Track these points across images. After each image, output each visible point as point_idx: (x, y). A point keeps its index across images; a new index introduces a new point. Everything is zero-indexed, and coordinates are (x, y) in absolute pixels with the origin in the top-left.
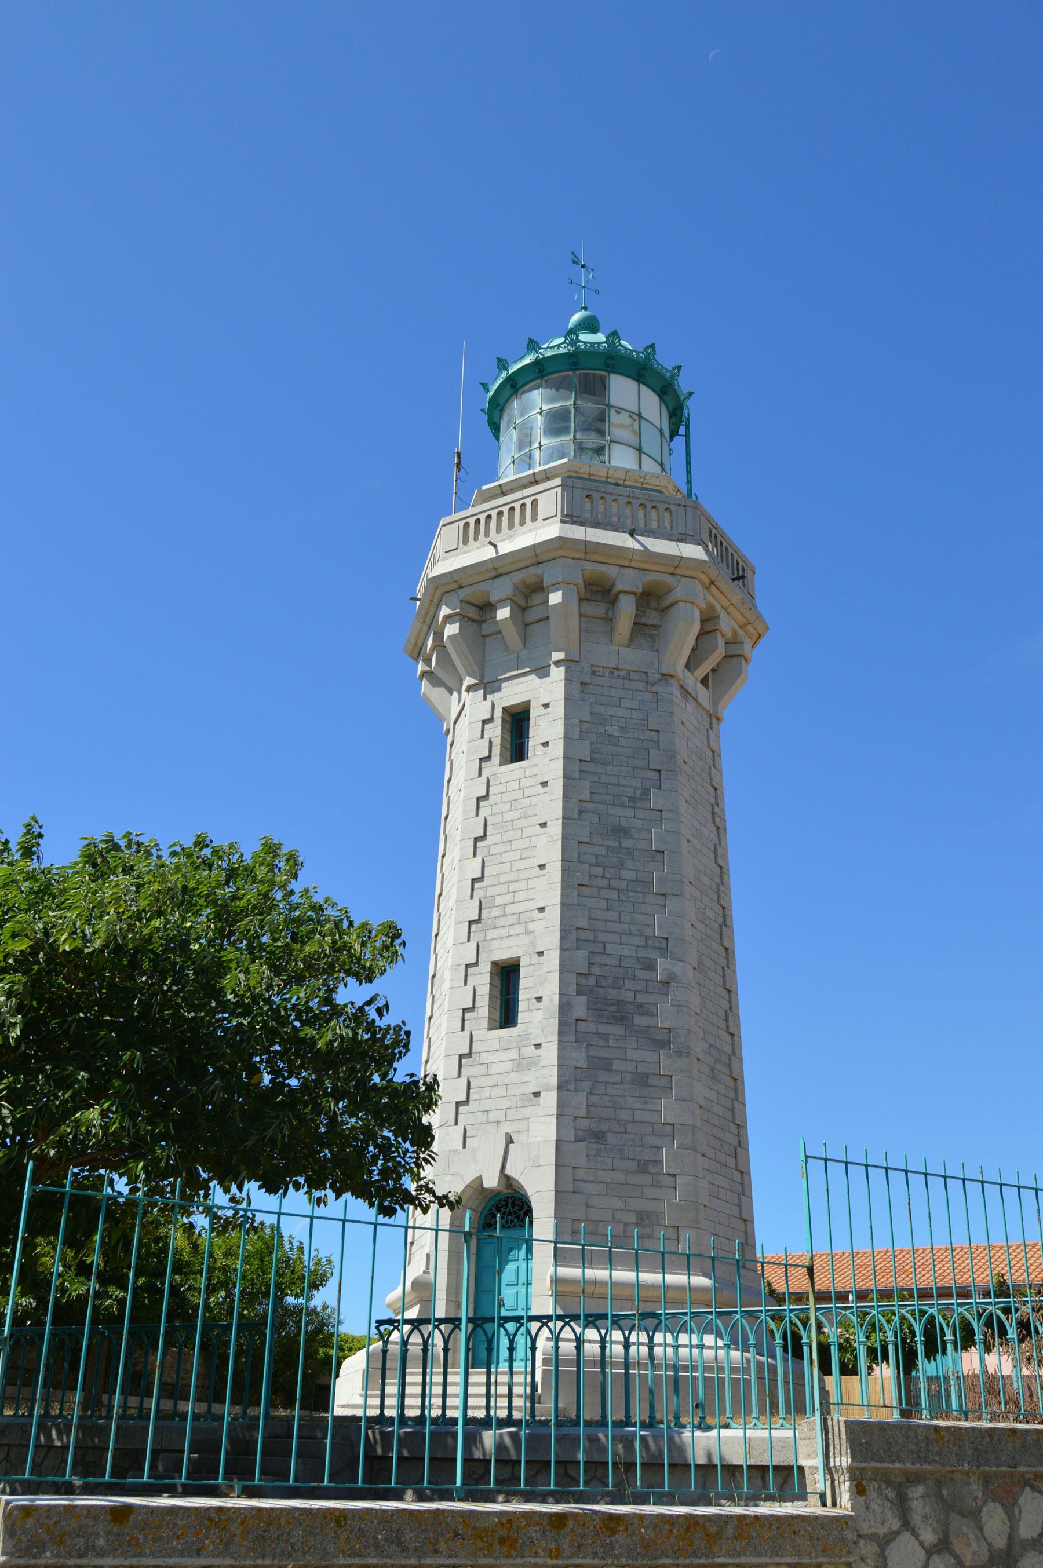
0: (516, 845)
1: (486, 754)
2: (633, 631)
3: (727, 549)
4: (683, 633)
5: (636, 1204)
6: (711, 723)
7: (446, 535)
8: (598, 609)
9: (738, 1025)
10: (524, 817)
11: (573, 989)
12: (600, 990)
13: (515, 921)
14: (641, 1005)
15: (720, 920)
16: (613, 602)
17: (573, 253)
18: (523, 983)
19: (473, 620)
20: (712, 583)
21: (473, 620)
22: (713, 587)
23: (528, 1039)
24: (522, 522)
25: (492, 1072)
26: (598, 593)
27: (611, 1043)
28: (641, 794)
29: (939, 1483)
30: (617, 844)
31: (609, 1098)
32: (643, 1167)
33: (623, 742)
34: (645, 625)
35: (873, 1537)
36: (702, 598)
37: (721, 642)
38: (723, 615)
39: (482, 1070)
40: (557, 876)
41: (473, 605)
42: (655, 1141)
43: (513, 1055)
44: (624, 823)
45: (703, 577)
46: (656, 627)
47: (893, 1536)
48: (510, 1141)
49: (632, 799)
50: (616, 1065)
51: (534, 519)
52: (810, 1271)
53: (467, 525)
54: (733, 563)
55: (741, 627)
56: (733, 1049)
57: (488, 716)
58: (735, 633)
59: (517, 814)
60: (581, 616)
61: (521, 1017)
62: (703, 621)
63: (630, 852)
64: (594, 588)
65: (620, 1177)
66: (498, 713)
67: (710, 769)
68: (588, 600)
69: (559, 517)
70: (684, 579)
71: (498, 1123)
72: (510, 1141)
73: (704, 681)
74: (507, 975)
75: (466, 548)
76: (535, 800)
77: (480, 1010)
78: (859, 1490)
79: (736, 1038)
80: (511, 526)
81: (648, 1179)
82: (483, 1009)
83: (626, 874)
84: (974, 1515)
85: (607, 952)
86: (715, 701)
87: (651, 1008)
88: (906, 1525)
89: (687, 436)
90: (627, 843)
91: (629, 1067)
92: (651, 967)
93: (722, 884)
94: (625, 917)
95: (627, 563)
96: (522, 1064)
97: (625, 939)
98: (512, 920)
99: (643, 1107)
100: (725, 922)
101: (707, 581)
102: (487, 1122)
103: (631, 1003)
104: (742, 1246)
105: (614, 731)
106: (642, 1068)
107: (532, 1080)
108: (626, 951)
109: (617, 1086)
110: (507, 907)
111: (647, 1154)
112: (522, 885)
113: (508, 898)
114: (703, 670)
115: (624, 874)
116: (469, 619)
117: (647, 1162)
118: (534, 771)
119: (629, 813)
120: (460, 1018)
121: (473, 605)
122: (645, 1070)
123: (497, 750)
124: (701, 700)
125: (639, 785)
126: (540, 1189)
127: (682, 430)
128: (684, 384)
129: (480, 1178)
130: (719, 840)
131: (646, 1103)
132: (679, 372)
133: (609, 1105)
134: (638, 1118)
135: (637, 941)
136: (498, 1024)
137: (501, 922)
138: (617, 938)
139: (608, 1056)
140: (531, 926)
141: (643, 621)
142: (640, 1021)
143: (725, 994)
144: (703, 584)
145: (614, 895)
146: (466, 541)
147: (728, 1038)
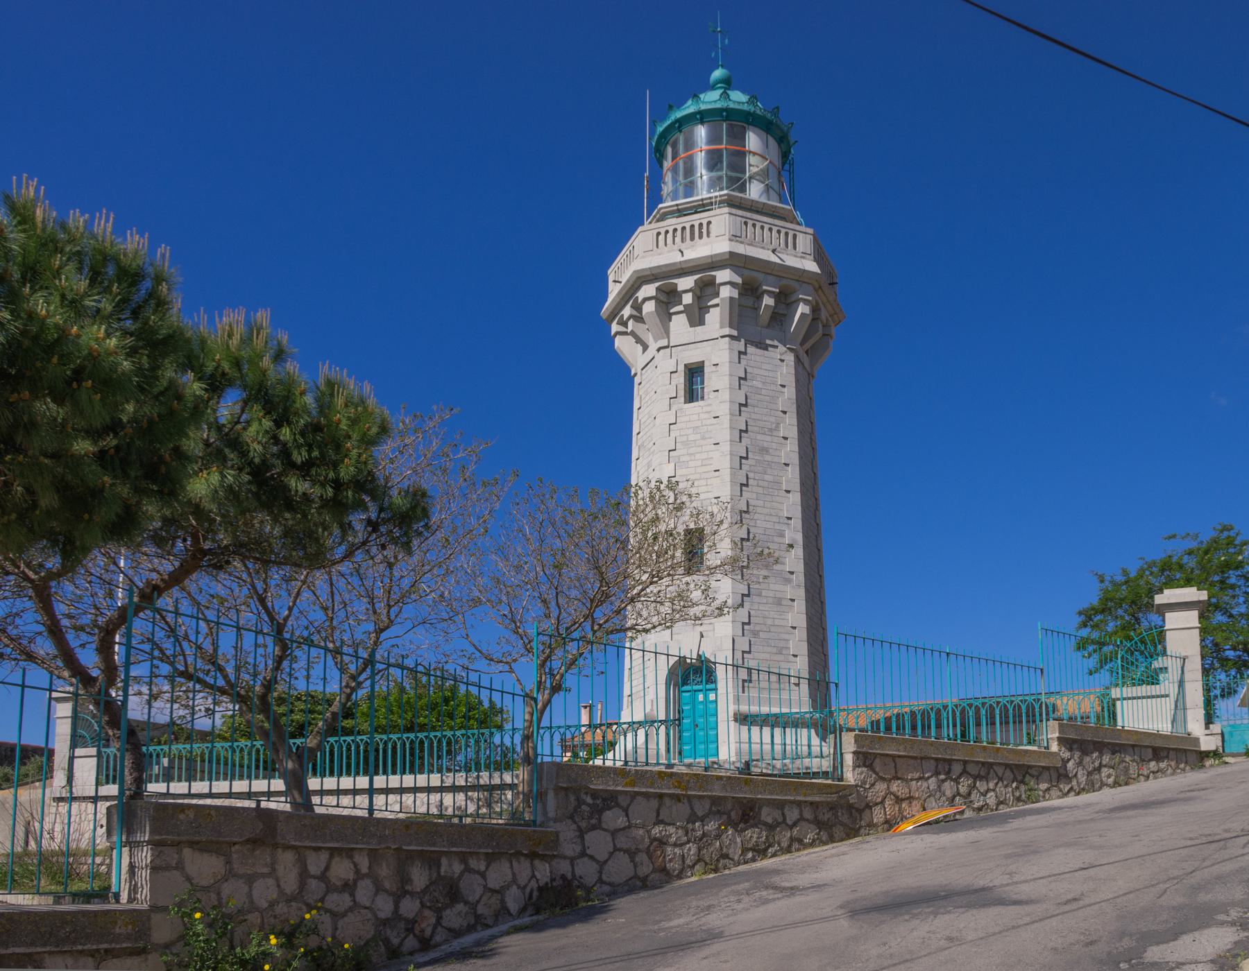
0: (698, 456)
8: (749, 301)
10: (703, 438)
26: (750, 290)
40: (727, 478)
42: (787, 637)
44: (765, 445)
46: (785, 315)
49: (771, 430)
59: (698, 436)
66: (681, 368)
69: (727, 237)
74: (694, 373)
100: (817, 509)
106: (778, 595)
111: (782, 644)
114: (807, 346)
115: (767, 477)
118: (708, 409)
119: (768, 438)
123: (681, 393)
135: (775, 519)
145: (760, 490)
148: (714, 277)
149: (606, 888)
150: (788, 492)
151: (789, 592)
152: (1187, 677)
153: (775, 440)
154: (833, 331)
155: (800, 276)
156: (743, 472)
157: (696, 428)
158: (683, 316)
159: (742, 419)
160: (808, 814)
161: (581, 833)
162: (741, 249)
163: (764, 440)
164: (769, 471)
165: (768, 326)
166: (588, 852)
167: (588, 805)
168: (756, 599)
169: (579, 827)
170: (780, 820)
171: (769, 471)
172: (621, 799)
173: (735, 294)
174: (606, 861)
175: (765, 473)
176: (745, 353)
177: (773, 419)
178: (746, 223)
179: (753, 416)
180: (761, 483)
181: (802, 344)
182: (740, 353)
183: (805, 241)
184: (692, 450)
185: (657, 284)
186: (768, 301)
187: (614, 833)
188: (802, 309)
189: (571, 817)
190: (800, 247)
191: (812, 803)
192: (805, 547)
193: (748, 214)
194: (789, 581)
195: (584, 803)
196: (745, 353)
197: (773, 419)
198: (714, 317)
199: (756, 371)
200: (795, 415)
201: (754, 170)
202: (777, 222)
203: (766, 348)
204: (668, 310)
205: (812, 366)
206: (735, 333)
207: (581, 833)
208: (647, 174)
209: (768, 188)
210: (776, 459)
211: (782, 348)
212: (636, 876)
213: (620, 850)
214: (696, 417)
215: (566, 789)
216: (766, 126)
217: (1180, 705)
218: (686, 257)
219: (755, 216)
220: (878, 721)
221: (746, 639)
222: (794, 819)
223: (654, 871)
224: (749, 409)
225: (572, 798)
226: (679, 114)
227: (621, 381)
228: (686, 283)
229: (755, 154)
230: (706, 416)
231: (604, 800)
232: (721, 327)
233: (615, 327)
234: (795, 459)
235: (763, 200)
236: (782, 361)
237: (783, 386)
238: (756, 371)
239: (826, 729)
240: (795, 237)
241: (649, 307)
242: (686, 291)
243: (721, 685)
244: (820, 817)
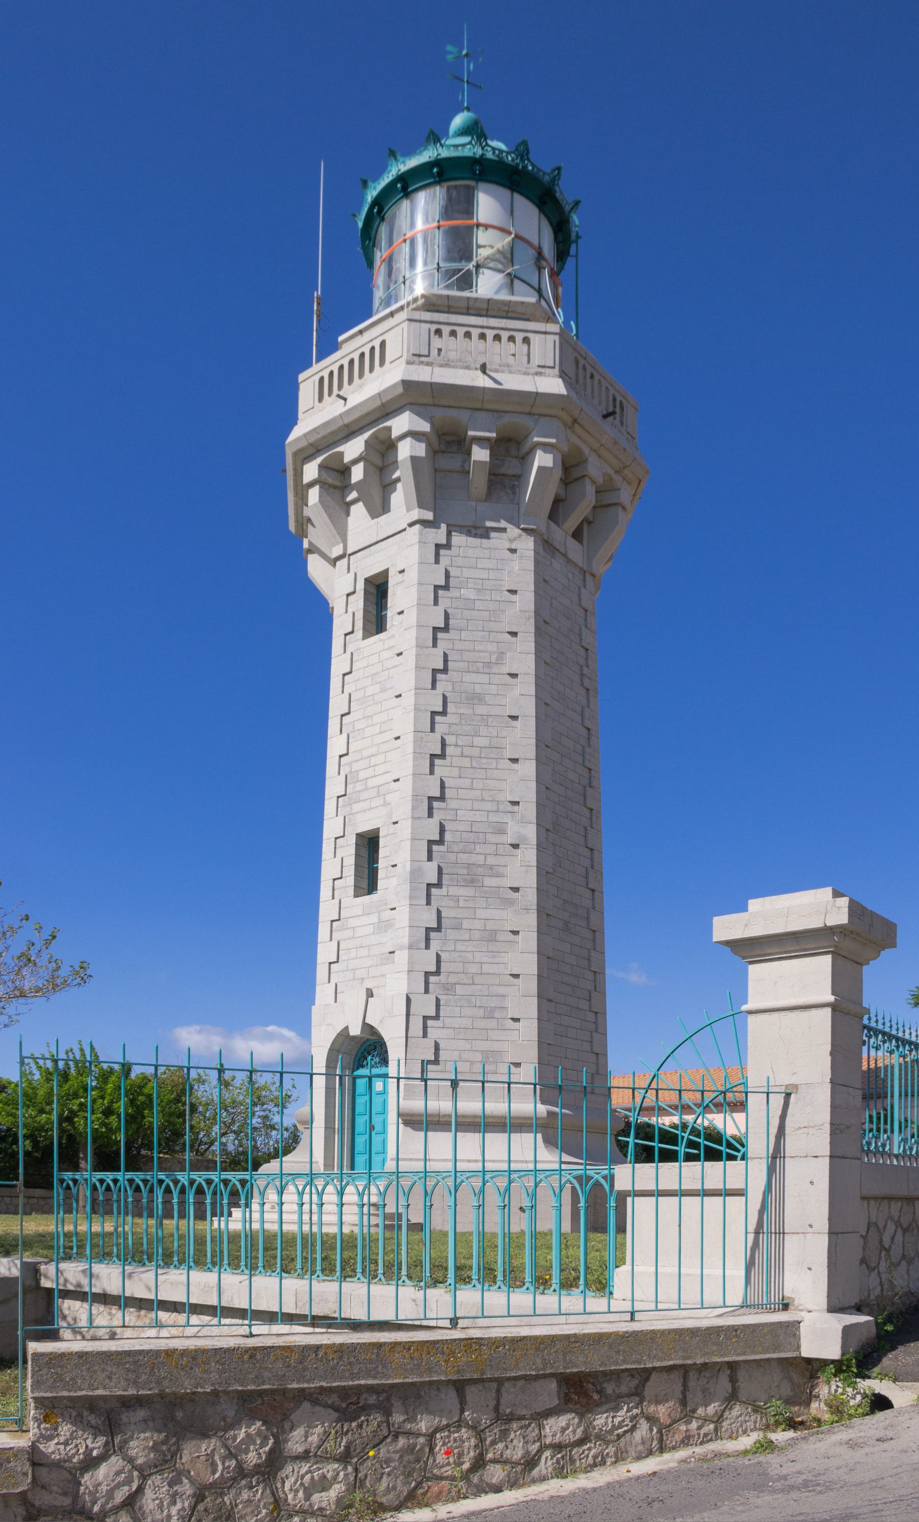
0: (377, 719)
1: (350, 630)
3: (600, 383)
5: (482, 1045)
6: (584, 580)
8: (452, 462)
9: (600, 882)
10: (383, 690)
12: (450, 855)
13: (375, 794)
14: (491, 867)
15: (585, 782)
18: (382, 852)
19: (335, 487)
20: (575, 421)
21: (335, 487)
22: (576, 426)
23: (386, 904)
24: (372, 369)
25: (357, 935)
26: (447, 443)
27: (461, 904)
28: (497, 660)
30: (471, 712)
31: (458, 954)
32: (489, 1014)
33: (478, 605)
34: (504, 475)
37: (590, 490)
38: (593, 460)
39: (349, 933)
40: (410, 748)
41: (333, 470)
42: (502, 990)
43: (374, 919)
44: (478, 689)
45: (563, 414)
48: (370, 994)
49: (488, 664)
50: (466, 924)
51: (382, 363)
54: (607, 398)
55: (617, 472)
56: (593, 904)
57: (352, 590)
59: (377, 688)
60: (436, 470)
61: (380, 884)
63: (485, 718)
64: (449, 439)
65: (467, 1023)
66: (361, 585)
67: (581, 630)
68: (443, 452)
69: (403, 360)
70: (542, 419)
71: (362, 979)
72: (370, 994)
73: (577, 535)
75: (321, 405)
77: (348, 879)
79: (596, 893)
81: (493, 1023)
82: (350, 879)
83: (480, 741)
85: (458, 818)
87: (501, 869)
90: (481, 709)
91: (478, 925)
92: (501, 830)
93: (589, 746)
94: (478, 784)
95: (479, 406)
96: (384, 926)
97: (476, 806)
98: (373, 793)
99: (490, 960)
101: (569, 420)
102: (354, 979)
103: (480, 866)
104: (592, 1077)
105: (472, 595)
106: (490, 926)
107: (388, 941)
108: (478, 816)
109: (467, 943)
110: (369, 781)
111: (493, 1003)
112: (381, 758)
113: (370, 772)
114: (572, 523)
115: (478, 741)
116: (330, 486)
117: (493, 1009)
119: (484, 678)
120: (331, 888)
121: (333, 470)
122: (493, 928)
123: (359, 624)
124: (571, 555)
125: (495, 649)
126: (393, 1035)
129: (347, 1028)
130: (588, 702)
131: (494, 957)
132: (559, 174)
133: (459, 959)
134: (484, 971)
135: (489, 806)
136: (366, 891)
137: (364, 795)
138: (469, 805)
139: (459, 916)
140: (388, 798)
141: (502, 471)
143: (587, 852)
144: (565, 424)
145: (466, 762)
146: (321, 399)
147: (588, 894)
150: (515, 761)
151: (510, 918)
152: (791, 1145)
154: (625, 496)
155: (533, 404)
156: (437, 736)
157: (414, 675)
158: (360, 504)
159: (438, 653)
162: (423, 374)
163: (476, 682)
164: (483, 731)
168: (451, 934)
171: (483, 731)
173: (421, 450)
175: (477, 734)
176: (448, 546)
177: (492, 647)
178: (438, 332)
179: (458, 645)
180: (467, 751)
182: (438, 547)
183: (545, 346)
185: (320, 460)
186: (480, 454)
188: (542, 460)
190: (536, 360)
193: (442, 317)
194: (510, 903)
196: (448, 546)
198: (401, 499)
199: (467, 573)
200: (531, 638)
201: (484, 253)
202: (493, 322)
203: (485, 534)
204: (344, 497)
206: (429, 516)
208: (318, 293)
209: (512, 278)
210: (496, 711)
211: (513, 531)
214: (375, 659)
216: (511, 177)
217: (768, 1230)
218: (351, 403)
219: (453, 318)
220: (214, 1214)
221: (431, 998)
224: (452, 634)
226: (371, 194)
228: (353, 449)
229: (487, 227)
234: (528, 708)
235: (504, 296)
236: (514, 551)
237: (513, 592)
238: (467, 573)
242: (355, 462)
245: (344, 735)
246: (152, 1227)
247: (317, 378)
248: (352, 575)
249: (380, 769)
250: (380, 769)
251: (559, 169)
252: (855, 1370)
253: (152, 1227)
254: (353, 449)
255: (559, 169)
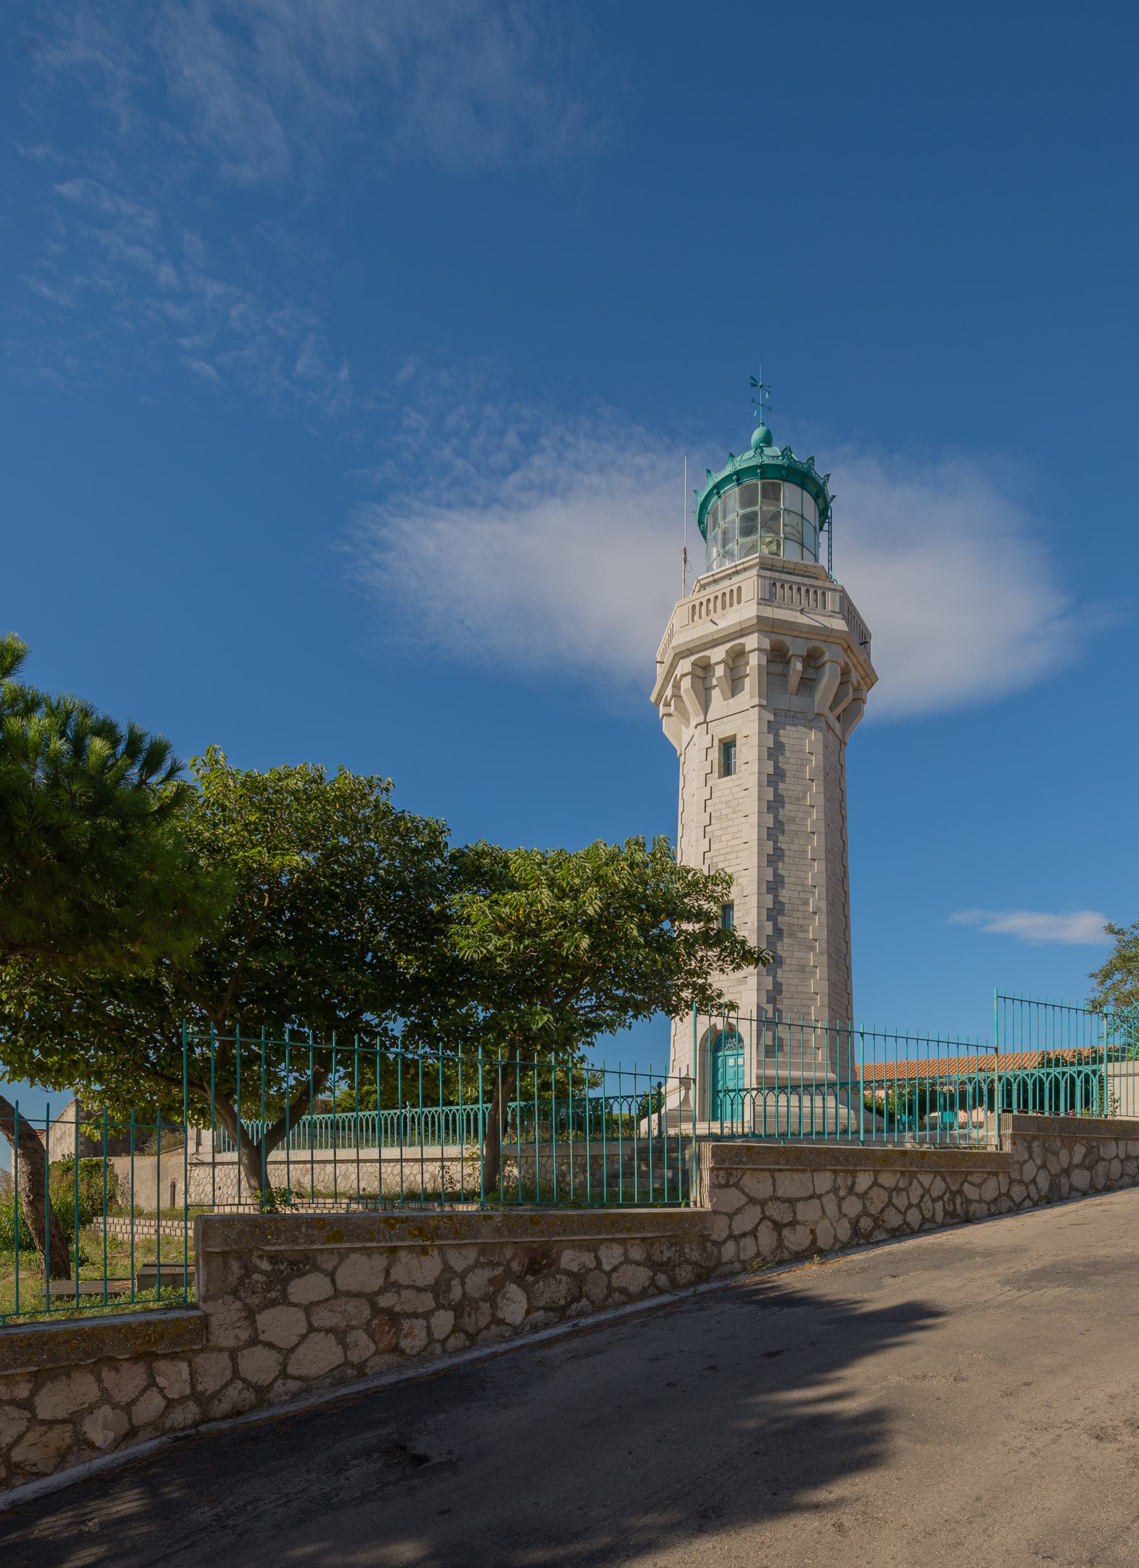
0: (730, 830)
2: (800, 684)
4: (828, 681)
7: (679, 616)
8: (778, 668)
10: (734, 812)
11: (765, 917)
14: (801, 926)
16: (788, 663)
17: (752, 378)
24: (731, 605)
26: (777, 656)
29: (1044, 1141)
35: (1018, 1162)
36: (843, 658)
37: (851, 689)
40: (755, 850)
42: (809, 1002)
44: (793, 814)
46: (814, 680)
47: (1026, 1161)
49: (798, 799)
51: (739, 602)
52: (996, 1049)
53: (694, 606)
58: (858, 683)
59: (730, 810)
62: (842, 675)
66: (716, 743)
69: (755, 601)
74: (728, 747)
76: (741, 801)
78: (1014, 1143)
80: (724, 608)
84: (1057, 1154)
86: (844, 731)
88: (1031, 1157)
89: (830, 532)
100: (845, 876)
101: (846, 646)
111: (804, 1010)
112: (733, 855)
114: (839, 710)
118: (740, 782)
119: (795, 808)
123: (716, 768)
127: (826, 527)
128: (831, 490)
135: (800, 888)
142: (801, 935)
148: (743, 645)
149: (293, 1385)
153: (802, 809)
160: (636, 1253)
161: (251, 1315)
165: (798, 692)
166: (262, 1337)
167: (265, 1273)
169: (245, 1305)
170: (591, 1264)
171: (796, 841)
172: (321, 1260)
174: (293, 1349)
175: (792, 842)
177: (799, 788)
178: (774, 584)
181: (832, 709)
184: (723, 825)
187: (308, 1309)
189: (235, 1293)
190: (829, 607)
191: (643, 1239)
192: (829, 914)
193: (777, 575)
195: (258, 1270)
197: (799, 788)
205: (843, 734)
206: (765, 703)
207: (251, 1315)
212: (347, 1363)
213: (318, 1330)
215: (224, 1254)
222: (615, 1262)
223: (378, 1352)
225: (235, 1265)
227: (668, 761)
230: (738, 789)
231: (292, 1264)
232: (752, 697)
233: (662, 710)
239: (845, 1087)
240: (824, 594)
241: (686, 683)
243: (747, 1050)
244: (657, 1257)
245: (707, 840)
246: (287, 1082)
247: (690, 605)
248: (710, 736)
249: (733, 862)
250: (733, 862)
251: (812, 458)
252: (215, 1031)
253: (287, 1082)
254: (717, 654)
255: (812, 458)
